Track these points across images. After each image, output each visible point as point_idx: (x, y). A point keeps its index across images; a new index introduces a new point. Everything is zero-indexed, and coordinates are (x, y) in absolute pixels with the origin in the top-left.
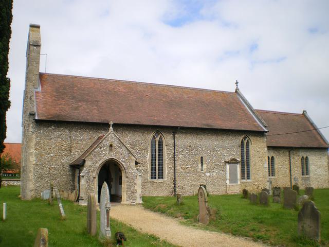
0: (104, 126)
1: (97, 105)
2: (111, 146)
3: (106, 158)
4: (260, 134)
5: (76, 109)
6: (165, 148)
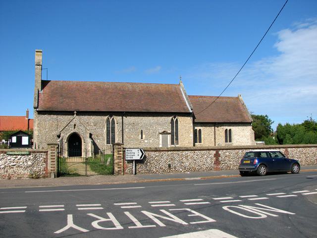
1: (75, 100)
2: (75, 125)
3: (72, 132)
4: (187, 114)
6: (116, 125)
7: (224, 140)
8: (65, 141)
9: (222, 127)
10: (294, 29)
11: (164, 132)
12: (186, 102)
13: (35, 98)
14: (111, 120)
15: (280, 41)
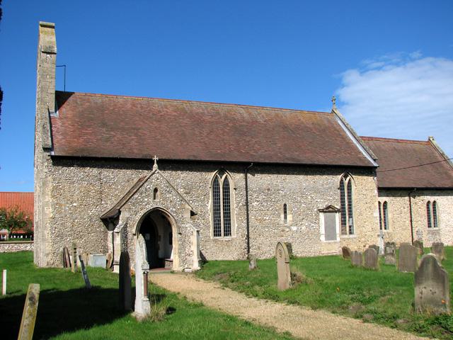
0: (145, 163)
2: (156, 190)
3: (149, 207)
4: (368, 170)
5: (107, 140)
6: (232, 192)
7: (427, 225)
8: (134, 231)
9: (422, 197)
10: (364, 70)
11: (329, 207)
12: (358, 146)
13: (44, 127)
14: (221, 181)
15: (343, 86)
